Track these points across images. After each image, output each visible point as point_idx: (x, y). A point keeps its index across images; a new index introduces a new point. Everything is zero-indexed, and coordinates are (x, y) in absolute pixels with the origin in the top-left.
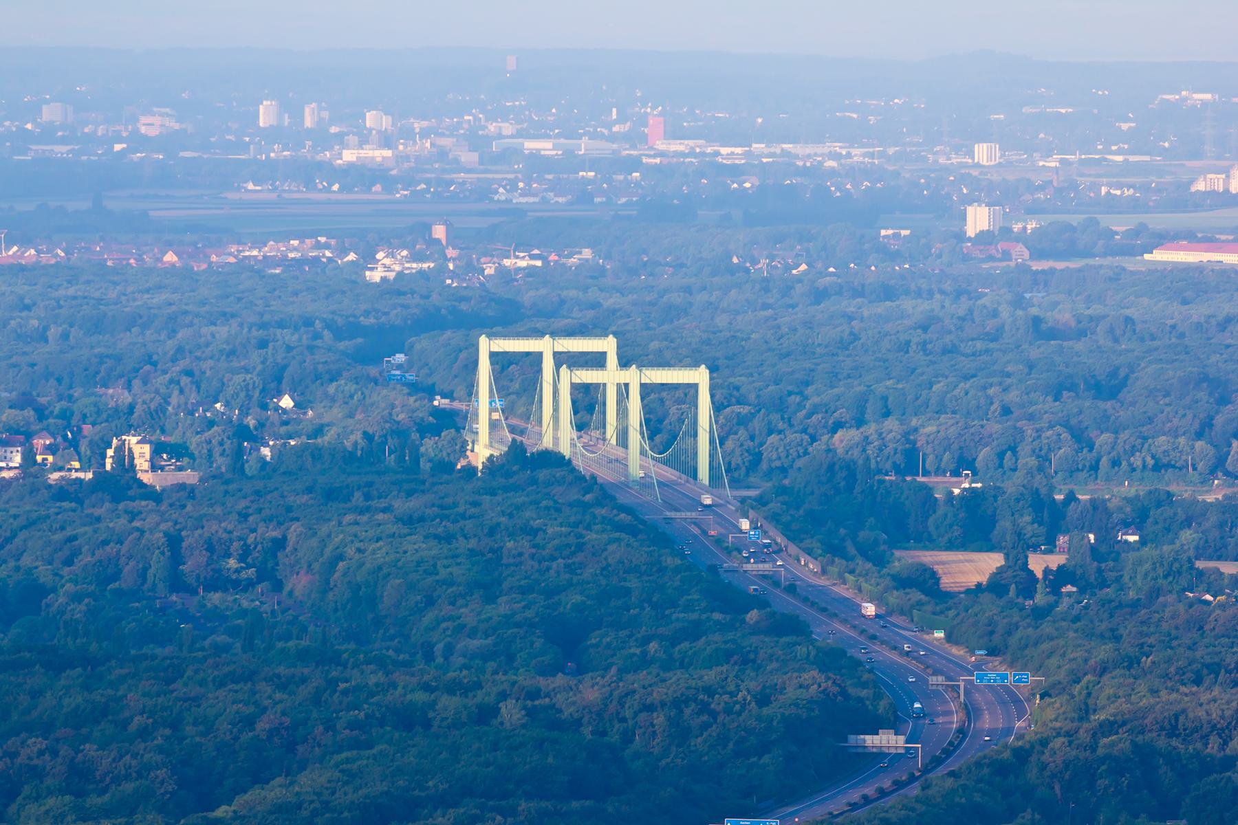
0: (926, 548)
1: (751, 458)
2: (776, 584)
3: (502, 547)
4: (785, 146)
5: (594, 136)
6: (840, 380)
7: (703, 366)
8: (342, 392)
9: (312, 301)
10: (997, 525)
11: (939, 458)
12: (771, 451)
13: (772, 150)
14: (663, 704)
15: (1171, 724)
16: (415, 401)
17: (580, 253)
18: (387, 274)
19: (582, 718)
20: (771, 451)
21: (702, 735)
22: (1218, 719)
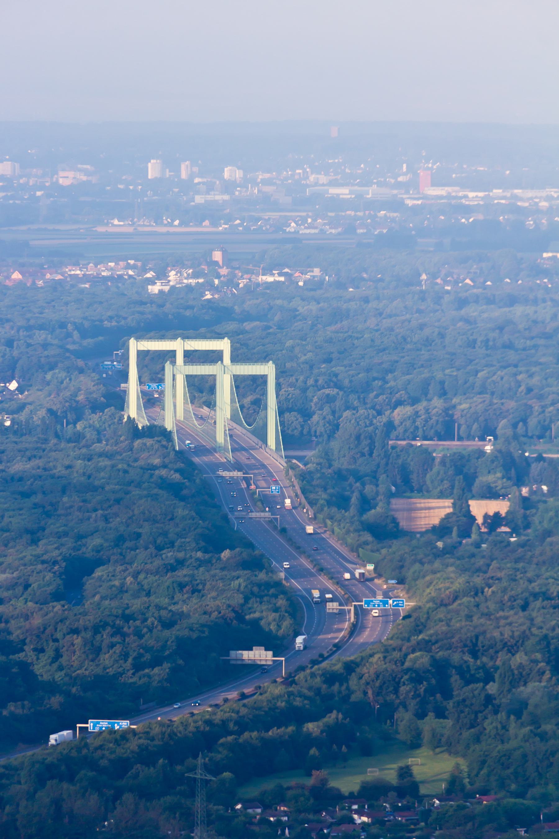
0: (423, 497)
1: (331, 427)
2: (275, 528)
3: (59, 502)
4: (516, 191)
5: (379, 184)
6: (415, 369)
7: (271, 362)
8: (57, 378)
9: (76, 309)
10: (477, 480)
11: (469, 427)
12: (346, 423)
13: (505, 194)
14: (86, 629)
15: (471, 641)
16: (94, 386)
17: (313, 271)
18: (164, 288)
19: (25, 639)
20: (346, 423)
21: (109, 652)
22: (509, 638)
